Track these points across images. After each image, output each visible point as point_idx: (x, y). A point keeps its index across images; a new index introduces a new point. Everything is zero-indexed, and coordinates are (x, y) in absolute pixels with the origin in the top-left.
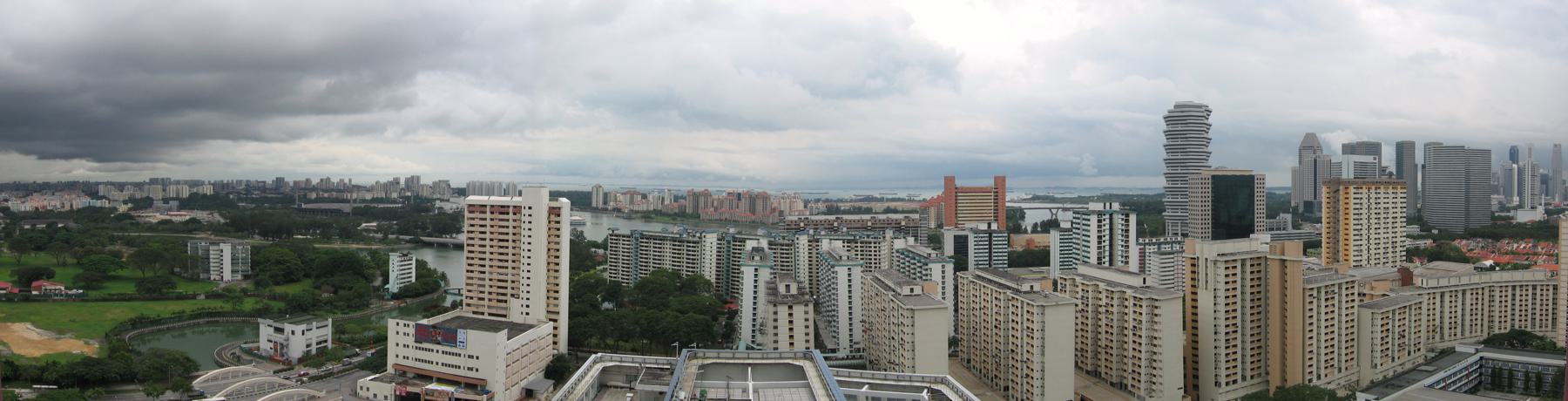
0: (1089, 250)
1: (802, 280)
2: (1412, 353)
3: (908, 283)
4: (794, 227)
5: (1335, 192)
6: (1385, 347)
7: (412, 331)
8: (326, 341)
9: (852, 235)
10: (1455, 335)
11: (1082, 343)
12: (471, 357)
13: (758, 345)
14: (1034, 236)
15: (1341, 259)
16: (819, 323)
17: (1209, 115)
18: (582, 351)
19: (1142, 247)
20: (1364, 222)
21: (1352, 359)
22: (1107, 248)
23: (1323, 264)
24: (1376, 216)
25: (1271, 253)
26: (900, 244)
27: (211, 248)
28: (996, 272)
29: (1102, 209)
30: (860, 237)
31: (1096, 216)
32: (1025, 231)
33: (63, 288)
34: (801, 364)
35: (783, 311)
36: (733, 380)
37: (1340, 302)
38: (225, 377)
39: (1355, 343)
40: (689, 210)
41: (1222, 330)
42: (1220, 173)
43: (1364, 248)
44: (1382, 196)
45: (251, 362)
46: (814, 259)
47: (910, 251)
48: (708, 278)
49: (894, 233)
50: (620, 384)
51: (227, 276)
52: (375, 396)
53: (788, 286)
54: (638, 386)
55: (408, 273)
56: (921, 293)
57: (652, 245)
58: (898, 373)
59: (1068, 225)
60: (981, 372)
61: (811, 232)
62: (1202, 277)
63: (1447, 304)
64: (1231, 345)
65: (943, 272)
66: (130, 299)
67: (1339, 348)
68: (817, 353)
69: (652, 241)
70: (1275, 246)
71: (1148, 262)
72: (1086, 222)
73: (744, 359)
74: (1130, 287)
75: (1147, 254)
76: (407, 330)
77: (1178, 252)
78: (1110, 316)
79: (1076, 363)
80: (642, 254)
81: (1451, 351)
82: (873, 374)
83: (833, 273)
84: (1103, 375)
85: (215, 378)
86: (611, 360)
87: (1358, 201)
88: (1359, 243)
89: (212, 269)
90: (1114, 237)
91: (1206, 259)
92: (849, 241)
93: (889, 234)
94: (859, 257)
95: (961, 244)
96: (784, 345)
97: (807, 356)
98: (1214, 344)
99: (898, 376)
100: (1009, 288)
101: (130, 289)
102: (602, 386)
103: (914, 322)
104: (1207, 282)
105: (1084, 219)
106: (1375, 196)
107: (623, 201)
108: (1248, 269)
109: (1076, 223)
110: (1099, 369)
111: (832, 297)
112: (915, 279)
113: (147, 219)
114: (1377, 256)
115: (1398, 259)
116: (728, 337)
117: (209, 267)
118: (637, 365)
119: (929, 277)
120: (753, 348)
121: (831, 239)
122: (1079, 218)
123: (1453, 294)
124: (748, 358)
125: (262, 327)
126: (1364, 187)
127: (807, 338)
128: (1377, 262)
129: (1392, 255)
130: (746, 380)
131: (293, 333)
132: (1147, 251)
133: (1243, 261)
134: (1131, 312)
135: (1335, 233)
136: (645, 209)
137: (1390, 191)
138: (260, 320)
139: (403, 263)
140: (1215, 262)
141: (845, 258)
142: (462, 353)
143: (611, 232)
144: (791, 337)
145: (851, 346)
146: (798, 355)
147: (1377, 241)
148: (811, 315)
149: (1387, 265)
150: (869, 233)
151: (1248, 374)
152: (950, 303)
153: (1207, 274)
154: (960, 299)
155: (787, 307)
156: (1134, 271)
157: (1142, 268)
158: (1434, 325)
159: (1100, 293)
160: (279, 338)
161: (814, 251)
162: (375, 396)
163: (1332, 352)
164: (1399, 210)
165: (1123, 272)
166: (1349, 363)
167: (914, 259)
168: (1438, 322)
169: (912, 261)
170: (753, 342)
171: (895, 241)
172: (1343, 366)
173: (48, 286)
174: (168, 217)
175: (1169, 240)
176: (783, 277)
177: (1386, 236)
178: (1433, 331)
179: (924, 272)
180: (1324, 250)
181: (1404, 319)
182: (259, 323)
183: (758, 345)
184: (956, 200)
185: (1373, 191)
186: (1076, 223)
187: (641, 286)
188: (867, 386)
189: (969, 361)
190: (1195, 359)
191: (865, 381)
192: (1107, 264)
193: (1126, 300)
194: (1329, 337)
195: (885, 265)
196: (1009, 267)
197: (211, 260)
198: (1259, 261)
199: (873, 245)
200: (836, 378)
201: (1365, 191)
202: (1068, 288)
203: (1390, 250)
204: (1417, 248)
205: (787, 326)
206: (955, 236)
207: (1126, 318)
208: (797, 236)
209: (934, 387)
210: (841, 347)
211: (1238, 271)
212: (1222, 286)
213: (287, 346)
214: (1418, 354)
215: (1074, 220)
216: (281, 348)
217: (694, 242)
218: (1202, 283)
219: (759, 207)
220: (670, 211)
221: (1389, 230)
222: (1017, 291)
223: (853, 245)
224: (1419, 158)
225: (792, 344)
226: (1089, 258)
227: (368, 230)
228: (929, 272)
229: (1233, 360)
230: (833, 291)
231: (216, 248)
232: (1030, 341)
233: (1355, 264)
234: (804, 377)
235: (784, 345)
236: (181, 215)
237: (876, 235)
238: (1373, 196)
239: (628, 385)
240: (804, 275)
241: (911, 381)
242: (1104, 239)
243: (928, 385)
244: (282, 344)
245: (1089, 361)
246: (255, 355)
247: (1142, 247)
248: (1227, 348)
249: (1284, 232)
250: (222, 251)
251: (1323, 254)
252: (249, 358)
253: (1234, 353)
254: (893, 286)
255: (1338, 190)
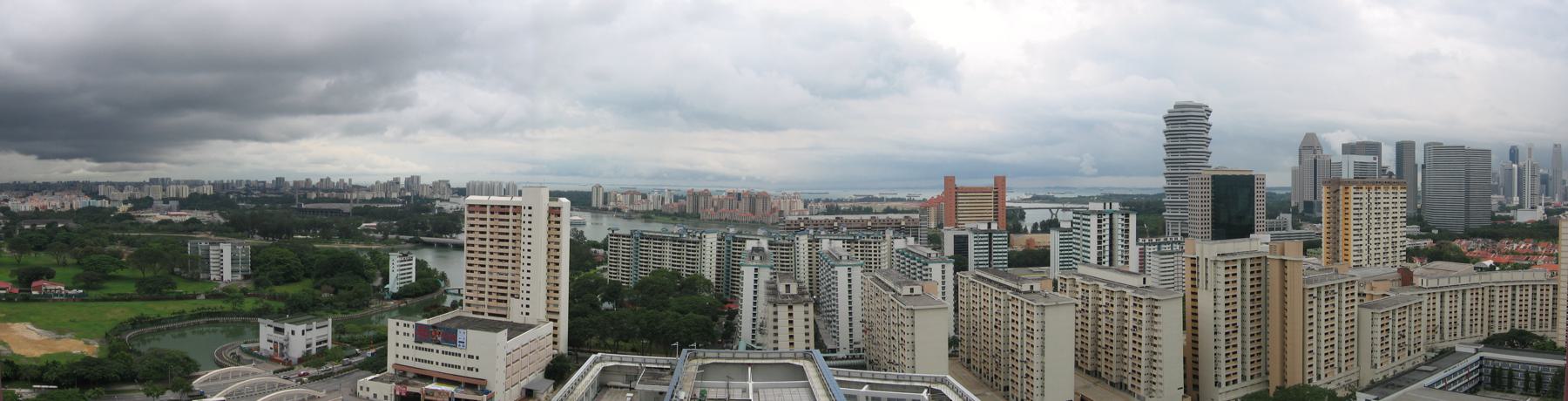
0: (1089, 250)
1: (802, 280)
2: (1412, 353)
3: (908, 283)
4: (794, 227)
5: (1335, 192)
6: (1385, 347)
7: (412, 331)
8: (326, 341)
9: (852, 235)
10: (1455, 335)
11: (1082, 343)
12: (471, 357)
13: (758, 345)
14: (1034, 236)
15: (1341, 259)
16: (819, 323)
17: (1209, 115)
18: (582, 351)
19: (1142, 247)
20: (1364, 222)
21: (1352, 359)
22: (1107, 248)
23: (1323, 264)
24: (1376, 216)
25: (1271, 253)
26: (900, 244)
27: (211, 248)
28: (996, 272)
29: (1102, 209)
30: (860, 237)
31: (1096, 216)
32: (1025, 231)
33: (63, 288)
34: (801, 364)
35: (783, 311)
36: (733, 380)
37: (1340, 302)
38: (225, 377)
39: (1355, 343)
40: (689, 210)
41: (1222, 330)
42: (1220, 173)
43: (1364, 248)
44: (1382, 196)
45: (251, 362)
46: (814, 259)
47: (910, 251)
48: (708, 278)
49: (894, 233)
50: (620, 384)
51: (227, 276)
52: (375, 396)
53: (788, 286)
54: (638, 386)
55: (408, 273)
56: (921, 293)
57: (652, 245)
58: (898, 373)
59: (1068, 225)
60: (981, 372)
61: (811, 232)
62: (1202, 277)
63: (1447, 304)
64: (1231, 345)
65: (943, 272)
66: (130, 299)
67: (1339, 348)
68: (817, 353)
69: (652, 241)
70: (1275, 246)
71: (1148, 262)
72: (1086, 222)
73: (744, 359)
74: (1130, 287)
75: (1147, 254)
76: (407, 330)
77: (1178, 252)
78: (1110, 316)
79: (1076, 363)
80: (642, 254)
81: (1451, 351)
82: (873, 374)
83: (833, 273)
84: (1103, 375)
85: (215, 378)
86: (611, 360)
87: (1358, 201)
88: (1359, 243)
89: (212, 269)
90: (1114, 237)
91: (1206, 259)
92: (849, 241)
93: (889, 234)
94: (859, 257)
95: (961, 244)
96: (784, 345)
97: (807, 356)
98: (1214, 344)
99: (898, 376)
100: (1009, 288)
101: (130, 289)
102: (602, 386)
103: (914, 322)
104: (1207, 282)
105: (1084, 219)
106: (1375, 196)
107: (623, 201)
108: (1248, 269)
109: (1076, 223)
110: (1099, 369)
111: (832, 297)
112: (915, 279)
113: (147, 219)
114: (1377, 256)
115: (1398, 259)
116: (728, 337)
117: (209, 267)
118: (637, 365)
119: (929, 277)
120: (753, 348)
121: (831, 239)
122: (1079, 218)
123: (1453, 294)
124: (748, 358)
125: (262, 327)
126: (1364, 187)
127: (807, 338)
128: (1377, 262)
129: (1392, 255)
130: (746, 380)
131: (293, 333)
132: (1147, 251)
133: (1243, 261)
134: (1131, 312)
135: (1335, 233)
136: (645, 209)
137: (1390, 191)
138: (260, 320)
139: (403, 263)
140: (1215, 262)
141: (845, 258)
142: (462, 353)
143: (611, 232)
144: (791, 337)
145: (851, 346)
146: (798, 355)
147: (1377, 241)
148: (811, 315)
149: (1387, 265)
150: (869, 233)
151: (1248, 374)
152: (950, 303)
153: (1207, 274)
154: (960, 299)
155: (787, 307)
156: (1134, 271)
157: (1142, 268)
158: (1434, 325)
159: (1100, 293)
160: (279, 338)
161: (814, 251)
162: (375, 396)
163: (1332, 352)
164: (1399, 210)
165: (1123, 272)
166: (1349, 363)
167: (914, 259)
168: (1438, 322)
169: (912, 261)
170: (753, 342)
171: (895, 241)
172: (1343, 366)
173: (48, 286)
174: (168, 217)
175: (1169, 240)
176: (783, 277)
177: (1386, 236)
178: (1433, 331)
179: (924, 272)
180: (1324, 250)
181: (1404, 319)
182: (259, 323)
183: (758, 345)
184: (956, 200)
185: (1373, 191)
186: (1076, 223)
187: (641, 286)
188: (867, 386)
189: (969, 361)
190: (1195, 359)
191: (865, 381)
192: (1107, 264)
193: (1126, 300)
194: (1329, 337)
195: (885, 265)
196: (1009, 267)
197: (211, 260)
198: (1259, 261)
199: (873, 245)
200: (836, 378)
201: (1365, 191)
202: (1068, 288)
203: (1390, 250)
204: (1417, 248)
205: (787, 326)
206: (955, 236)
207: (1126, 318)
208: (797, 236)
209: (934, 387)
210: (841, 347)
211: (1238, 271)
212: (1222, 286)
213: (287, 346)
214: (1418, 354)
215: (1074, 220)
216: (281, 348)
217: (694, 242)
218: (1202, 283)
219: (759, 207)
220: (670, 211)
221: (1389, 230)
222: (1017, 291)
223: (853, 245)
224: (1419, 158)
225: (792, 344)
226: (1089, 258)
227: (368, 230)
228: (929, 272)
229: (1233, 360)
230: (833, 291)
231: (216, 248)
232: (1030, 341)
233: (1355, 264)
234: (804, 377)
235: (784, 345)
236: (181, 215)
237: (876, 235)
238: (1373, 196)
239: (628, 385)
240: (804, 275)
241: (911, 381)
242: (1104, 239)
243: (928, 385)
244: (282, 344)
245: (1089, 361)
246: (255, 355)
247: (1142, 247)
248: (1227, 348)
249: (1284, 232)
250: (222, 251)
251: (1323, 254)
252: (249, 358)
253: (1234, 353)
254: (893, 286)
255: (1338, 190)
